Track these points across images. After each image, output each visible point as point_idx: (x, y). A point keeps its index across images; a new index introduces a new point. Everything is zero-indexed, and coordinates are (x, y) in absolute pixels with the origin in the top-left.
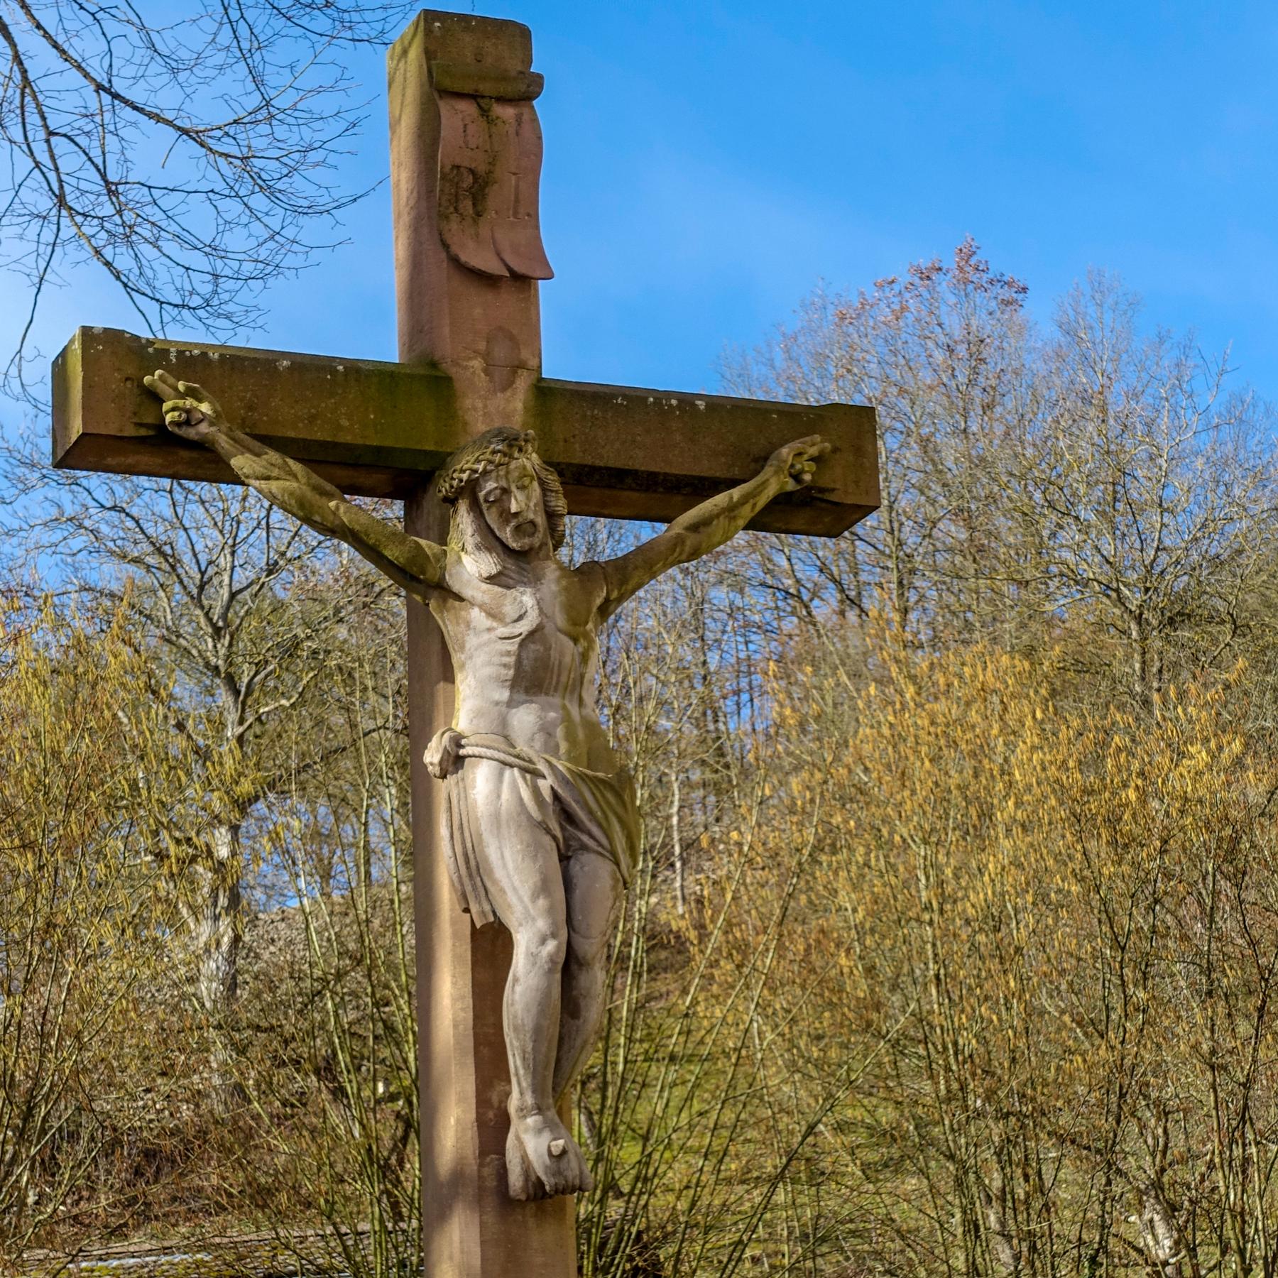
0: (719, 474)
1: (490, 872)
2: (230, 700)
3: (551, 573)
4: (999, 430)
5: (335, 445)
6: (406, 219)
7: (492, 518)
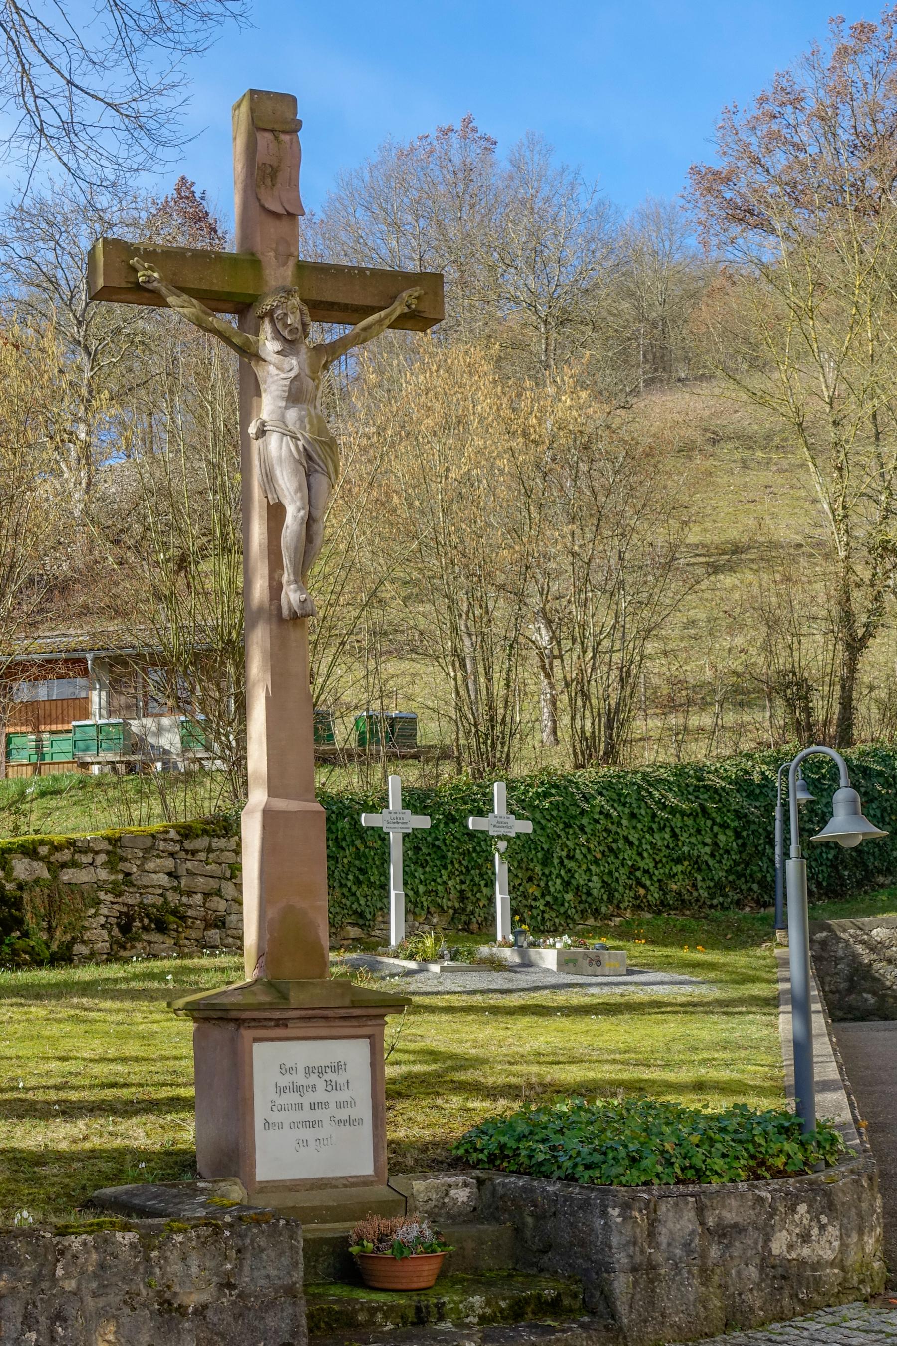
0: (375, 304)
1: (277, 481)
2: (86, 358)
3: (303, 350)
4: (478, 218)
5: (211, 291)
6: (240, 186)
7: (279, 326)
